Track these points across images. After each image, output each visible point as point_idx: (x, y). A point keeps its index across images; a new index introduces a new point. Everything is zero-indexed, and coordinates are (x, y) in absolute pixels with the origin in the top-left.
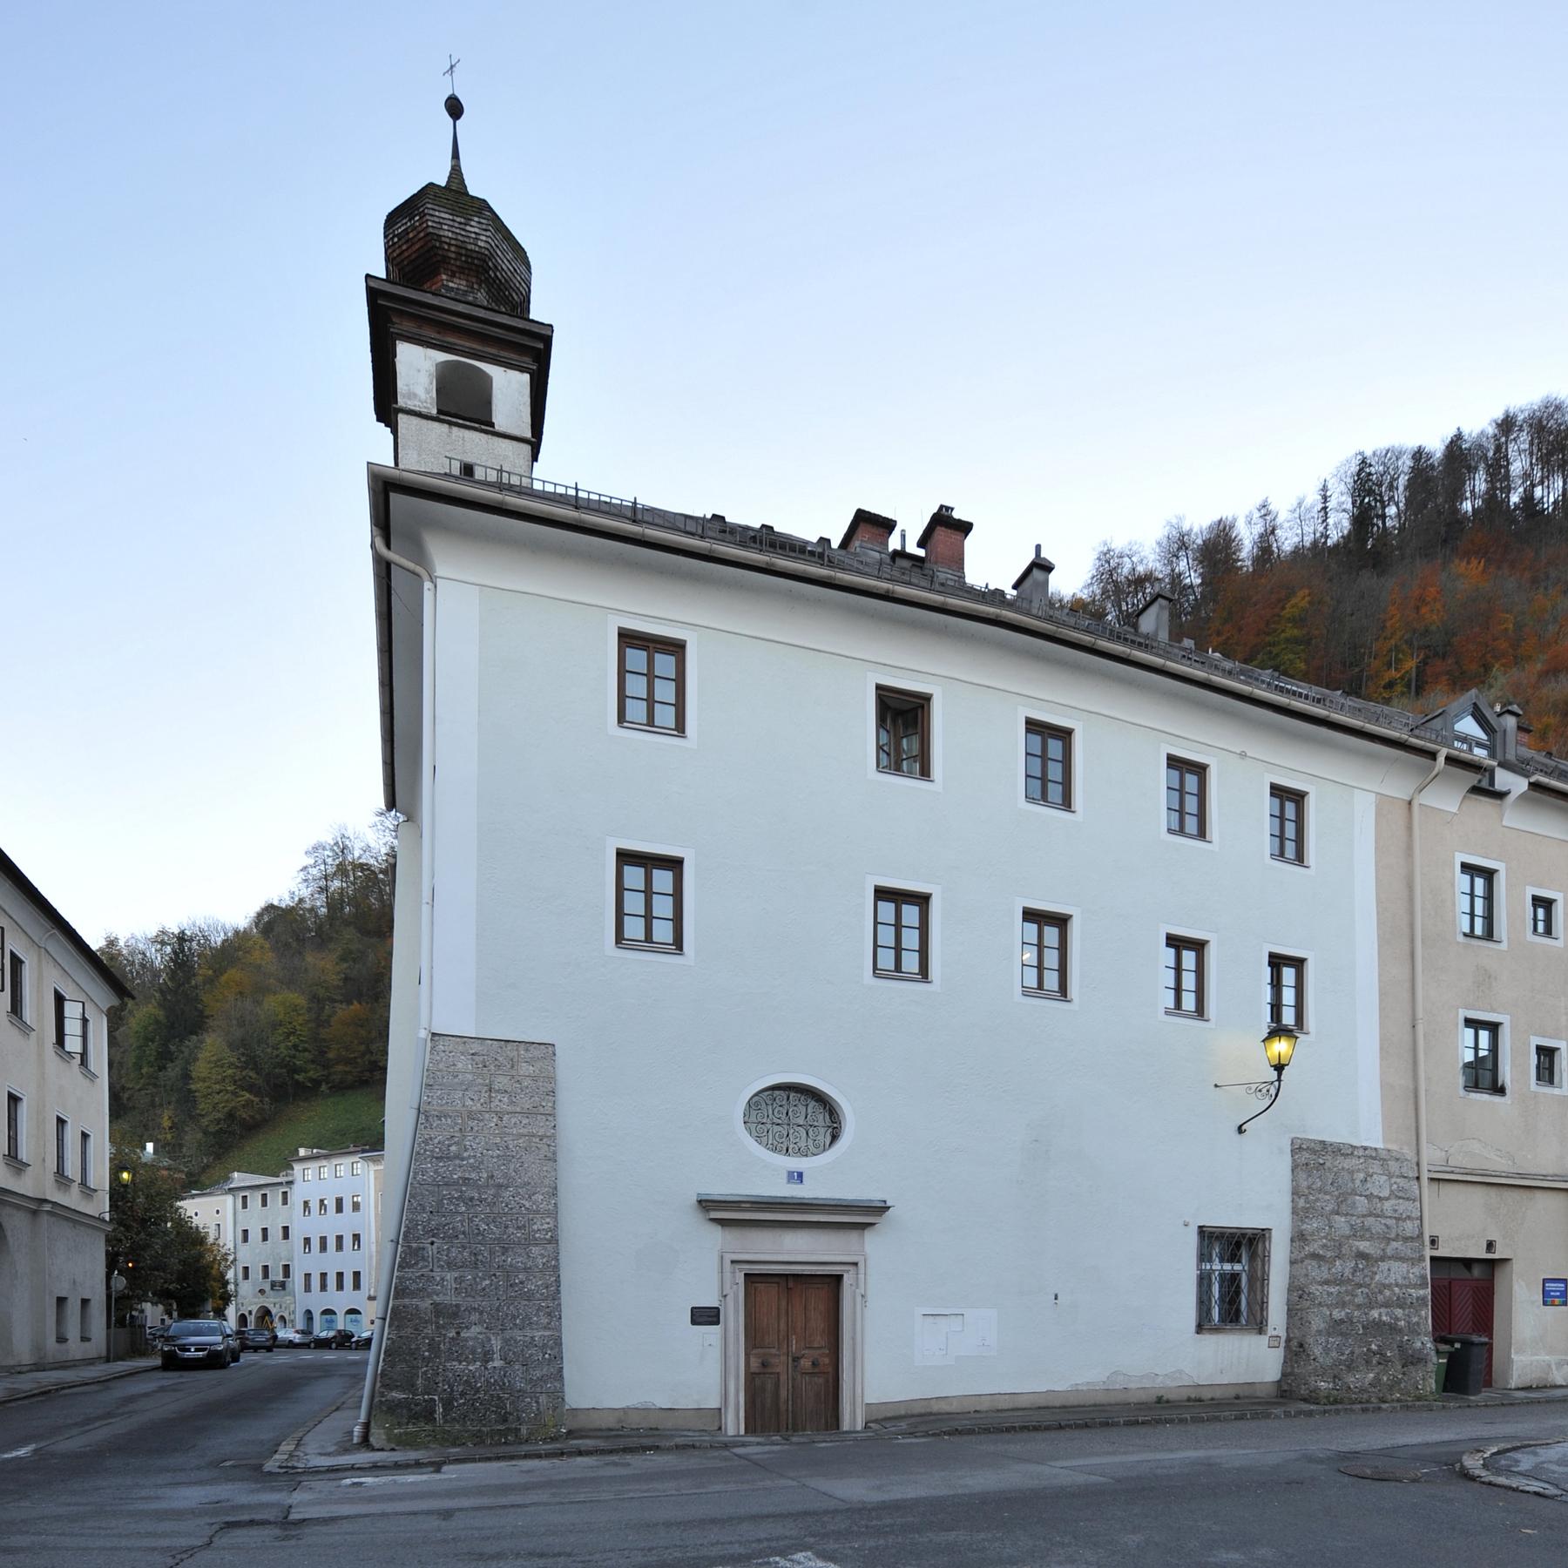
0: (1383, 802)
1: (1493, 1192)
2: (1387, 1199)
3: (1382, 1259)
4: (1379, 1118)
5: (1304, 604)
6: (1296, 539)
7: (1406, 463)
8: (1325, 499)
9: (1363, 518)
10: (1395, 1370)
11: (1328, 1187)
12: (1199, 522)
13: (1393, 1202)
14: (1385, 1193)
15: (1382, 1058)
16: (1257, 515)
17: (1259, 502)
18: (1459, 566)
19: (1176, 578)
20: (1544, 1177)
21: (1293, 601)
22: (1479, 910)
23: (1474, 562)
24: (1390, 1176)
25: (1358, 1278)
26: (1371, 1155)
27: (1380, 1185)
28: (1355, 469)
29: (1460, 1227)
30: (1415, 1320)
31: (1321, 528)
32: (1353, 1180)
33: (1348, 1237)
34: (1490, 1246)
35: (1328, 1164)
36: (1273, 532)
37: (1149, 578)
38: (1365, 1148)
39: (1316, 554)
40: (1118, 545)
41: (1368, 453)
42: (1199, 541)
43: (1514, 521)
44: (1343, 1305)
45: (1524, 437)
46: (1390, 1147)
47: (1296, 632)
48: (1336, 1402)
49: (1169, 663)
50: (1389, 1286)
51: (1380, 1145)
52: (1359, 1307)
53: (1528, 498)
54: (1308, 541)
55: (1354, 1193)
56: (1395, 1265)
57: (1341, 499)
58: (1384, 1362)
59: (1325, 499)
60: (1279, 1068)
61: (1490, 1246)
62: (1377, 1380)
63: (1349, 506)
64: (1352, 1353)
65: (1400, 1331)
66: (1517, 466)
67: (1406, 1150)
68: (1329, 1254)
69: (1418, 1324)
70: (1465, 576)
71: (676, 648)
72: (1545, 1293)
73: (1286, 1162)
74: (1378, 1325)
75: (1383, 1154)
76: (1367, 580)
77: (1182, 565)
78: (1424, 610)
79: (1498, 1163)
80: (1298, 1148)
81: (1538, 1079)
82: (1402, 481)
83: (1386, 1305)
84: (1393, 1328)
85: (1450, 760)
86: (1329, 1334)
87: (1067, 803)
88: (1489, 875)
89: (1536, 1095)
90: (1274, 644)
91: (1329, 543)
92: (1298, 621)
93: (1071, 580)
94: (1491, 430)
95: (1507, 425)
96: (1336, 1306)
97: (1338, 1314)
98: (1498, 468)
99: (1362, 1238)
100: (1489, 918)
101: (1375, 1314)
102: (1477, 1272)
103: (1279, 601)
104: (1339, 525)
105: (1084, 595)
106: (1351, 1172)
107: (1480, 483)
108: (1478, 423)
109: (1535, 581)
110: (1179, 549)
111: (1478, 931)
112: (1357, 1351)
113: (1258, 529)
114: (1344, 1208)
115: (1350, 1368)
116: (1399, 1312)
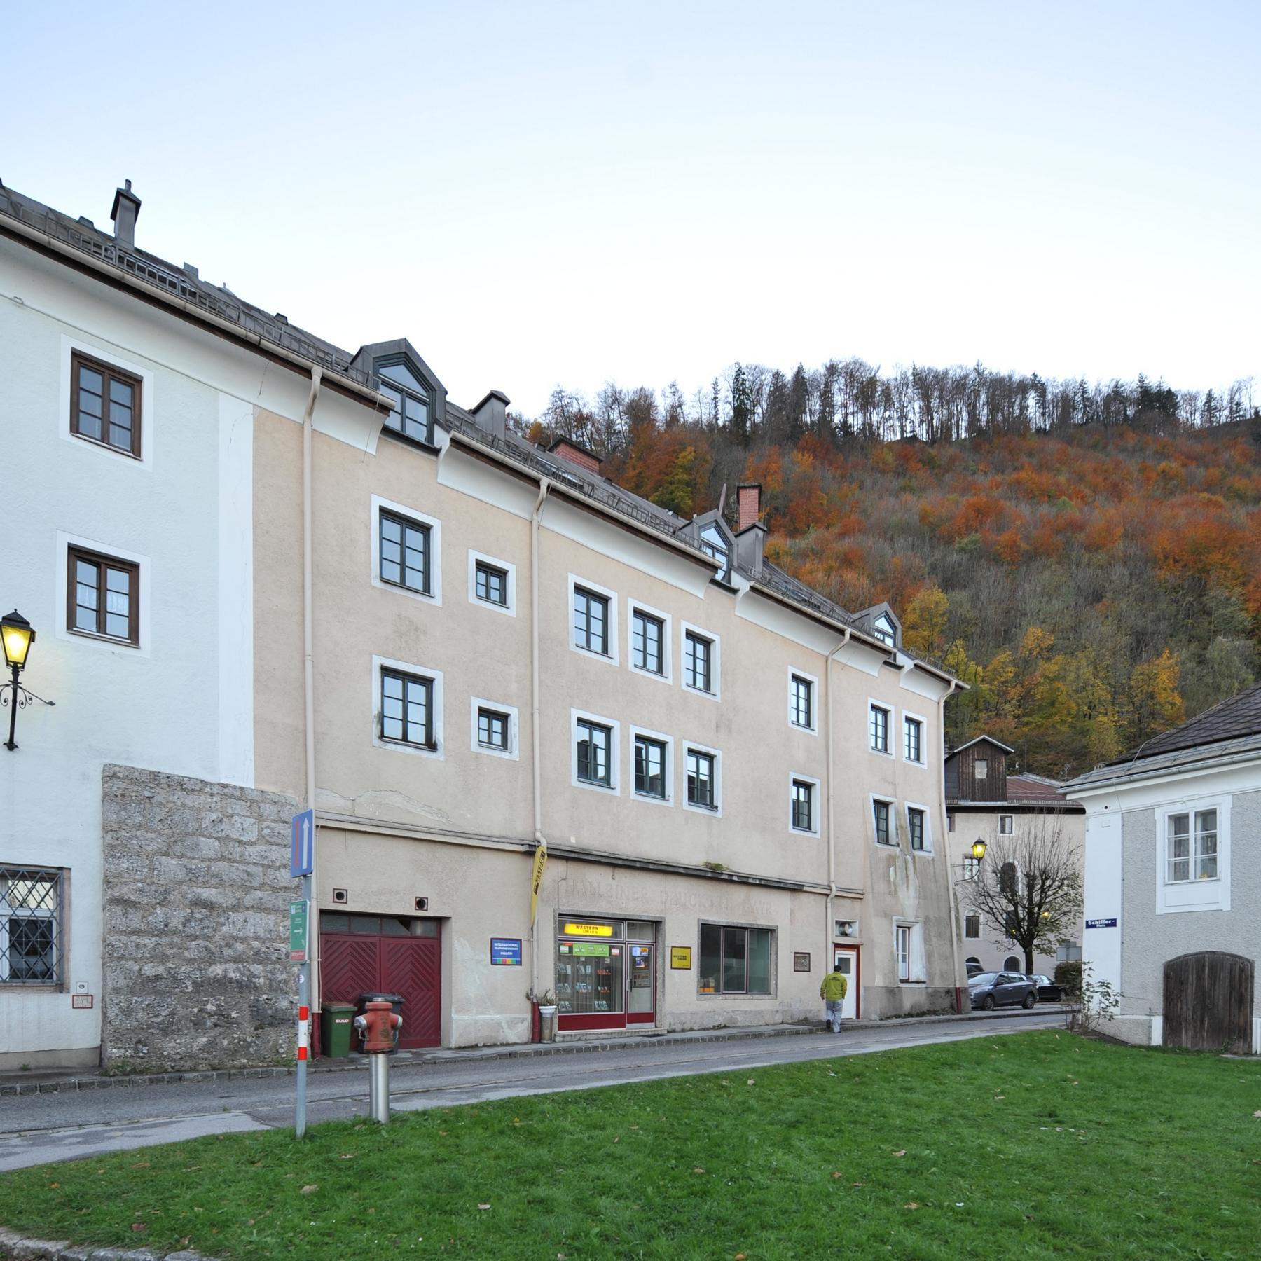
0: (263, 422)
1: (423, 848)
2: (252, 844)
3: (235, 909)
4: (251, 755)
5: (691, 457)
6: (697, 416)
7: (768, 378)
8: (716, 392)
9: (741, 413)
10: (246, 1032)
11: (155, 825)
12: (628, 388)
13: (259, 848)
14: (252, 837)
15: (256, 692)
16: (669, 391)
17: (671, 382)
18: (798, 456)
19: (611, 423)
20: (488, 838)
21: (683, 454)
22: (880, 734)
23: (807, 455)
24: (261, 819)
25: (193, 928)
26: (228, 793)
27: (243, 826)
28: (734, 374)
29: (381, 883)
30: (280, 977)
31: (713, 412)
32: (199, 820)
33: (180, 883)
34: (421, 903)
35: (158, 798)
36: (680, 406)
37: (589, 417)
38: (224, 786)
39: (708, 431)
40: (569, 390)
41: (743, 366)
42: (627, 400)
43: (835, 435)
44: (164, 958)
45: (842, 380)
46: (265, 788)
47: (685, 477)
48: (134, 1072)
49: (53, 241)
50: (244, 940)
51: (249, 784)
52: (190, 961)
53: (845, 422)
54: (705, 420)
55: (199, 832)
56: (254, 917)
57: (726, 392)
58: (223, 1020)
59: (716, 392)
60: (16, 668)
61: (421, 903)
62: (213, 1044)
63: (731, 399)
64: (172, 1014)
65: (257, 989)
66: (838, 399)
67: (290, 793)
68: (145, 900)
69: (286, 982)
70: (799, 462)
71: (133, 382)
72: (493, 953)
73: (95, 789)
74: (222, 983)
75: (254, 796)
76: (738, 453)
77: (615, 415)
78: (769, 478)
79: (425, 818)
80: (111, 776)
81: (691, 798)
82: (766, 390)
83: (236, 960)
84: (245, 986)
85: (552, 490)
86: (133, 992)
87: (135, 451)
88: (707, 643)
89: (478, 756)
90: (671, 483)
91: (720, 423)
92: (688, 470)
93: (531, 407)
94: (823, 371)
95: (832, 370)
96: (152, 959)
97: (150, 969)
98: (826, 396)
99: (206, 884)
100: (918, 749)
101: (217, 970)
102: (419, 929)
103: (674, 451)
104: (725, 413)
105: (543, 421)
106: (197, 811)
107: (815, 404)
108: (815, 367)
109: (843, 477)
110: (613, 402)
111: (880, 746)
112: (181, 1012)
113: (670, 401)
114: (178, 849)
115: (167, 1029)
116: (257, 969)
